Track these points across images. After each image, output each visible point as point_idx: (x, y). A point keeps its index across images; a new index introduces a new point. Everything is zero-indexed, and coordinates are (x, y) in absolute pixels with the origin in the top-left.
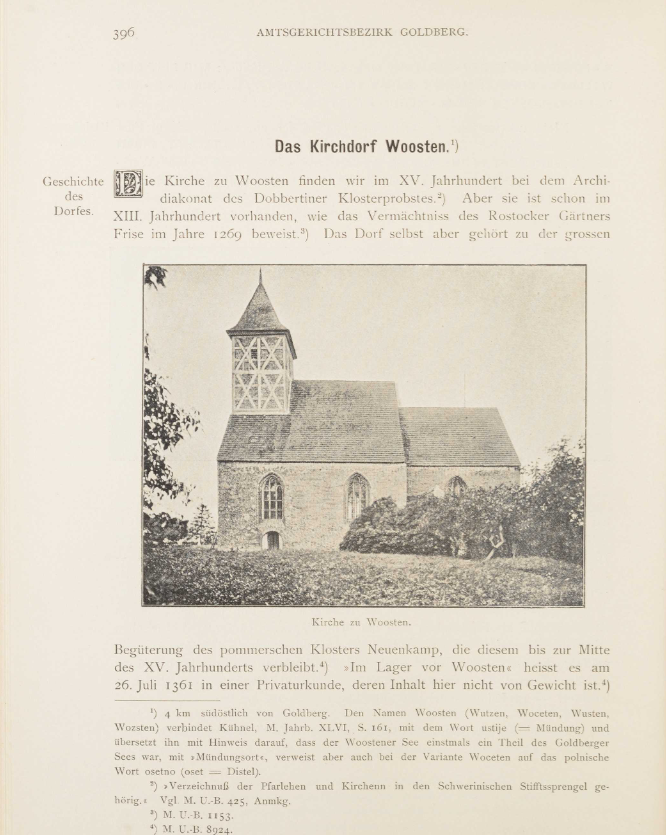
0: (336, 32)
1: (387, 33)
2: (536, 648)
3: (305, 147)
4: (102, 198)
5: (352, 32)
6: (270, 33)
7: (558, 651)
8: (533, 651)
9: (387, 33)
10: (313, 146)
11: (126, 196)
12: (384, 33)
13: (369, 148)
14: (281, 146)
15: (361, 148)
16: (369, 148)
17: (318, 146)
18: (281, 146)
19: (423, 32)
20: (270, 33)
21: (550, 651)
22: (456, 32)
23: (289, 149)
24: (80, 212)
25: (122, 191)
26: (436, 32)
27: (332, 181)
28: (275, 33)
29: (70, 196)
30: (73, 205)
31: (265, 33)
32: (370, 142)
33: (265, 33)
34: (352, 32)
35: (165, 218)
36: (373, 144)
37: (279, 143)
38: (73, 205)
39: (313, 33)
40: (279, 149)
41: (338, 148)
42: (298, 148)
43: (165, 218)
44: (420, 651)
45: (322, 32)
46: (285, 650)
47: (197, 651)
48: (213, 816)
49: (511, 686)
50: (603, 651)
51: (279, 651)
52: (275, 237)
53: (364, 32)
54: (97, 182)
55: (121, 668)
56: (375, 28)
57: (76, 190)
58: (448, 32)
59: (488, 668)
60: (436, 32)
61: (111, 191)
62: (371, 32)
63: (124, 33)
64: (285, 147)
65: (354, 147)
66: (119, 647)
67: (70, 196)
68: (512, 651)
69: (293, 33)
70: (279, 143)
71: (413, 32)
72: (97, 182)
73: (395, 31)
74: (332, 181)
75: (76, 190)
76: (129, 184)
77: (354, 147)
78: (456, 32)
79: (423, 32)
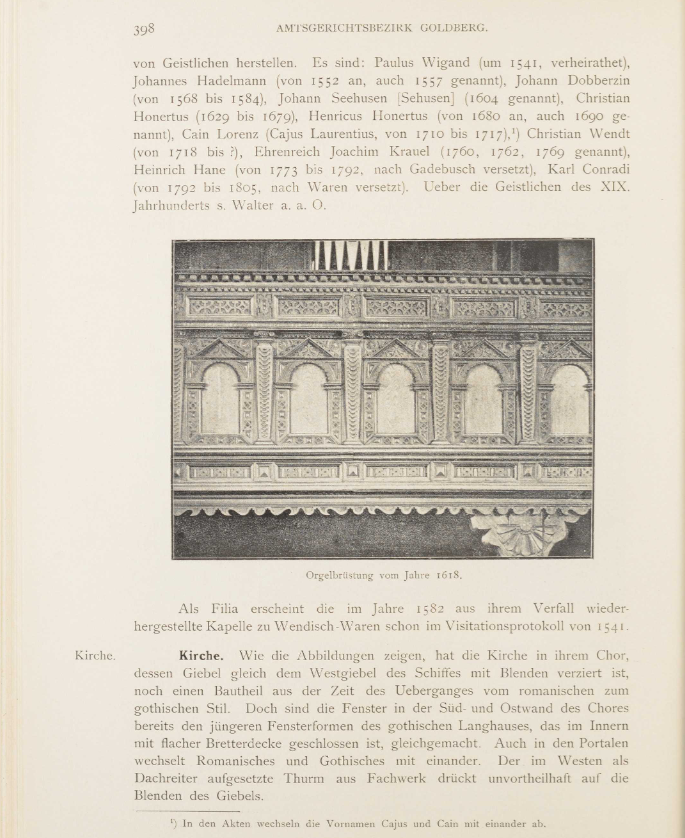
1: (407, 28)
2: (215, 150)
6: (289, 28)
7: (263, 628)
8: (210, 100)
9: (407, 28)
12: (404, 28)
19: (443, 27)
20: (289, 28)
21: (331, 63)
22: (475, 28)
26: (456, 28)
28: (295, 28)
33: (284, 28)
44: (451, 762)
45: (341, 28)
46: (211, 63)
47: (306, 692)
50: (299, 727)
51: (253, 762)
53: (384, 28)
55: (621, 674)
58: (324, 28)
59: (419, 98)
60: (456, 28)
66: (219, 688)
68: (494, 780)
71: (433, 28)
73: (415, 28)
78: (475, 28)
79: (443, 27)
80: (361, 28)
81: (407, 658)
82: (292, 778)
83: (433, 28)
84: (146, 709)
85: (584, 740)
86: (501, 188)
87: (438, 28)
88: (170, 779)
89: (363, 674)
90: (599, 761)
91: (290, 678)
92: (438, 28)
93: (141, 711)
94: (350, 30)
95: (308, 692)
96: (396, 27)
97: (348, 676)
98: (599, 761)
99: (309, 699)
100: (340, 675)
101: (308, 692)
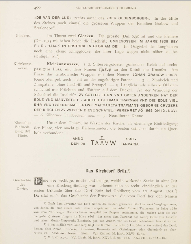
0: (99, 8)
1: (114, 8)
3: (94, 171)
4: (31, 185)
5: (103, 8)
9: (114, 8)
10: (97, 171)
11: (38, 184)
13: (113, 171)
14: (88, 171)
15: (110, 171)
16: (113, 171)
17: (98, 171)
18: (88, 171)
19: (124, 8)
22: (133, 8)
23: (90, 172)
24: (24, 189)
25: (36, 183)
27: (55, 181)
28: (81, 8)
29: (21, 185)
30: (22, 187)
31: (78, 8)
32: (113, 170)
33: (78, 8)
34: (103, 8)
35: (119, 181)
36: (114, 170)
37: (87, 170)
38: (22, 187)
39: (92, 8)
40: (87, 171)
41: (104, 171)
42: (92, 171)
43: (119, 181)
45: (95, 8)
48: (89, 204)
49: (131, 196)
52: (114, 181)
53: (107, 8)
54: (30, 181)
56: (110, 7)
57: (23, 183)
58: (90, 8)
61: (33, 184)
62: (109, 8)
63: (136, 37)
64: (89, 171)
65: (108, 171)
67: (21, 185)
69: (86, 8)
70: (87, 170)
71: (121, 8)
72: (30, 181)
73: (116, 8)
74: (55, 181)
75: (23, 183)
76: (39, 181)
77: (108, 171)
78: (133, 8)
79: (124, 8)
80: (100, 8)
81: (133, 53)
82: (57, 35)
83: (121, 8)
84: (129, 65)
85: (122, 79)
86: (79, 36)
87: (122, 8)
88: (108, 52)
89: (143, 47)
90: (74, 90)
91: (175, 198)
92: (122, 8)
93: (128, 65)
94: (97, 8)
95: (145, 70)
96: (110, 8)
97: (139, 47)
98: (74, 90)
99: (145, 193)
100: (137, 47)
101: (145, 70)
